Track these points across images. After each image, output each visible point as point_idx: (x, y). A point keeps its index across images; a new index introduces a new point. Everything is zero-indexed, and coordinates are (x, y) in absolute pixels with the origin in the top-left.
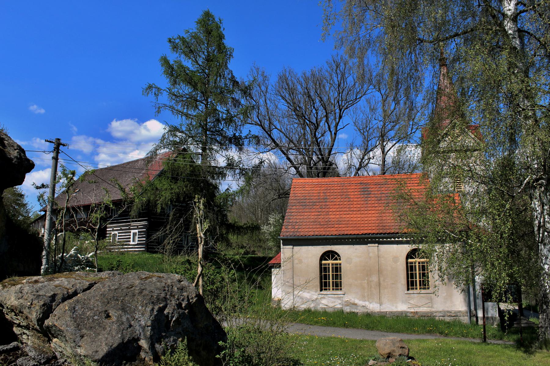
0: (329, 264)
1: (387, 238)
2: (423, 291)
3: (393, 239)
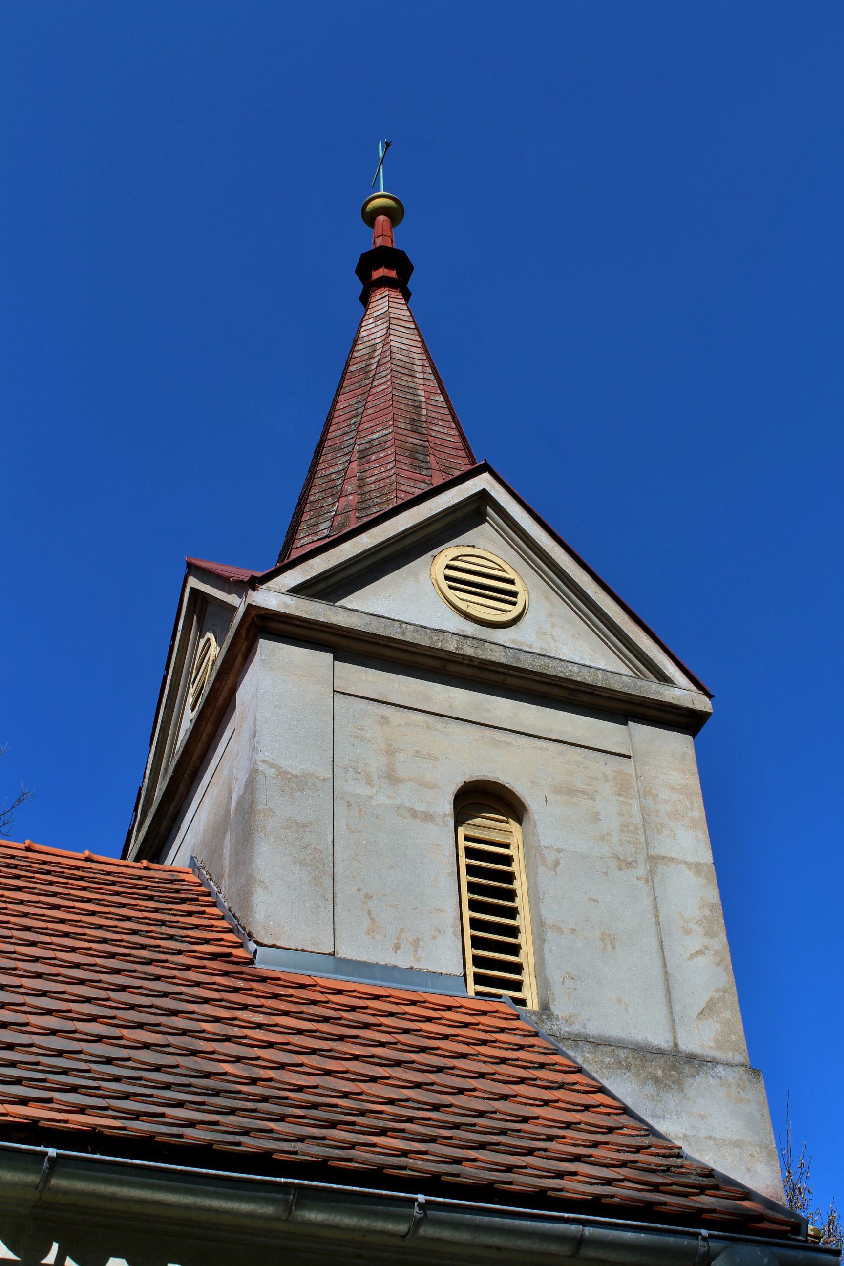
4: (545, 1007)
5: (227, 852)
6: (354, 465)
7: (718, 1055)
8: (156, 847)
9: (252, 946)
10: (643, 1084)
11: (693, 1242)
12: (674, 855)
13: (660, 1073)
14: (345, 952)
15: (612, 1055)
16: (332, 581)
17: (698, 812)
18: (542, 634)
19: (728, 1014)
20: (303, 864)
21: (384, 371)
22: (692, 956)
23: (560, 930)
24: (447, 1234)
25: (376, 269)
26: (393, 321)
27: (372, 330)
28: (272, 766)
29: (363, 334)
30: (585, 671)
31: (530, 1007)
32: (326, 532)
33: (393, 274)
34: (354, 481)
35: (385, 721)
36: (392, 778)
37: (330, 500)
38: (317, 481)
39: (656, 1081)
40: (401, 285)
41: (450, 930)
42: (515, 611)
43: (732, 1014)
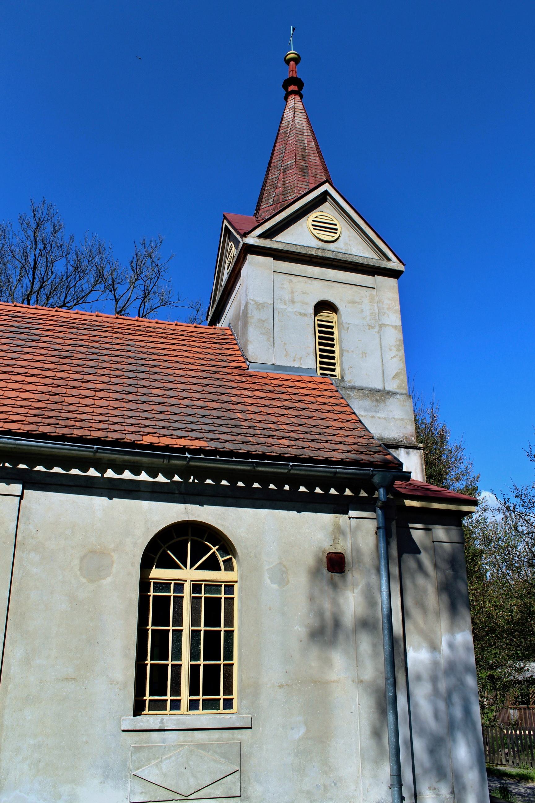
1: (67, 463)
2: (204, 718)
3: (92, 472)
4: (342, 377)
5: (240, 327)
6: (281, 175)
7: (398, 391)
8: (216, 319)
9: (248, 363)
10: (373, 402)
11: (368, 472)
12: (388, 323)
13: (378, 398)
14: (277, 363)
15: (363, 393)
16: (272, 230)
17: (398, 307)
18: (346, 244)
19: (402, 377)
20: (264, 334)
21: (292, 134)
22: (392, 358)
23: (348, 351)
24: (298, 472)
25: (290, 86)
26: (296, 110)
27: (288, 114)
28: (253, 300)
29: (285, 116)
30: (360, 258)
31: (337, 377)
32: (271, 203)
33: (296, 88)
34: (281, 182)
35: (291, 281)
36: (293, 302)
37: (273, 190)
38: (269, 181)
39: (377, 400)
40: (298, 93)
41: (312, 354)
42: (336, 236)
43: (404, 377)
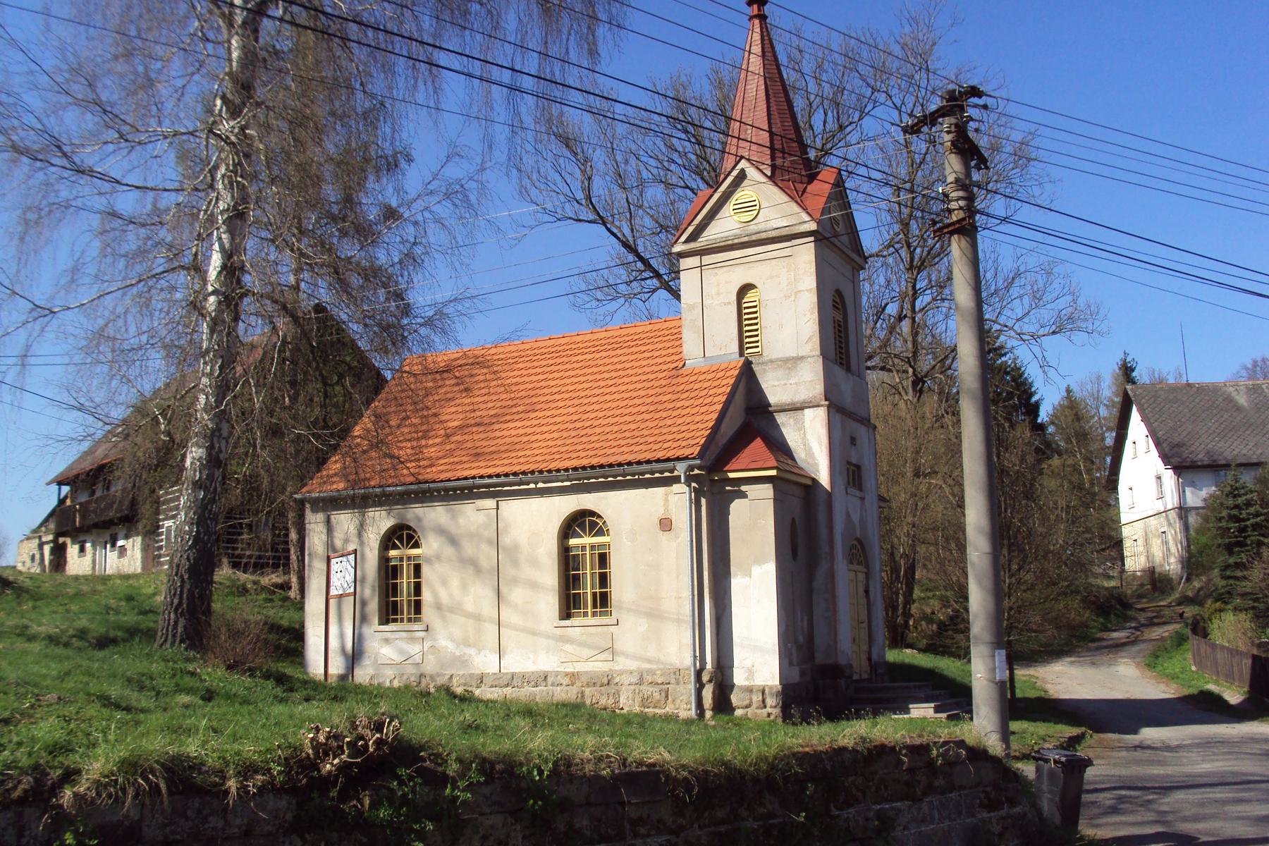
0: (584, 548)
